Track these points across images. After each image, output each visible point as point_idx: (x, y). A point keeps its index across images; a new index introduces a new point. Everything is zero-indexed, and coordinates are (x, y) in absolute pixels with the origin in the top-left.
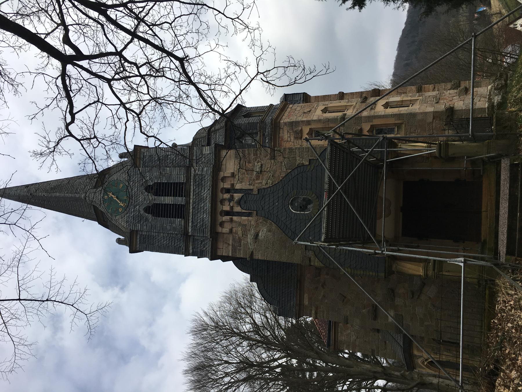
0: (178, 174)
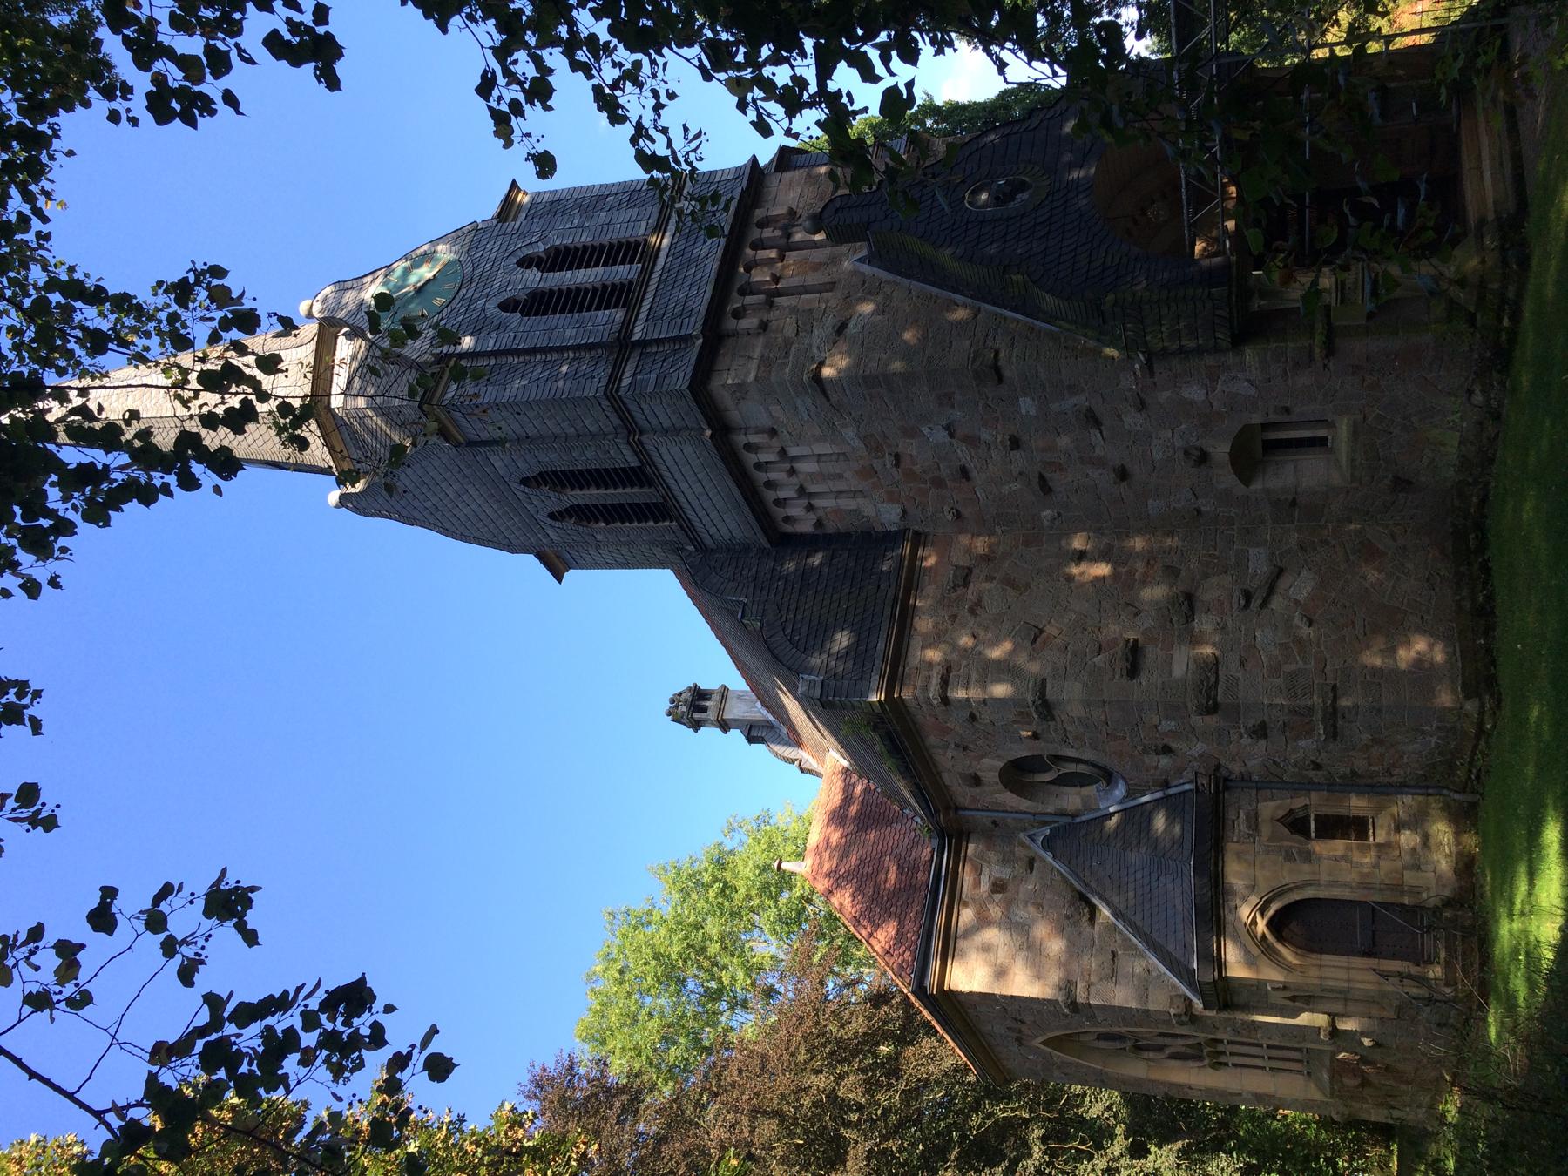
0: (632, 219)
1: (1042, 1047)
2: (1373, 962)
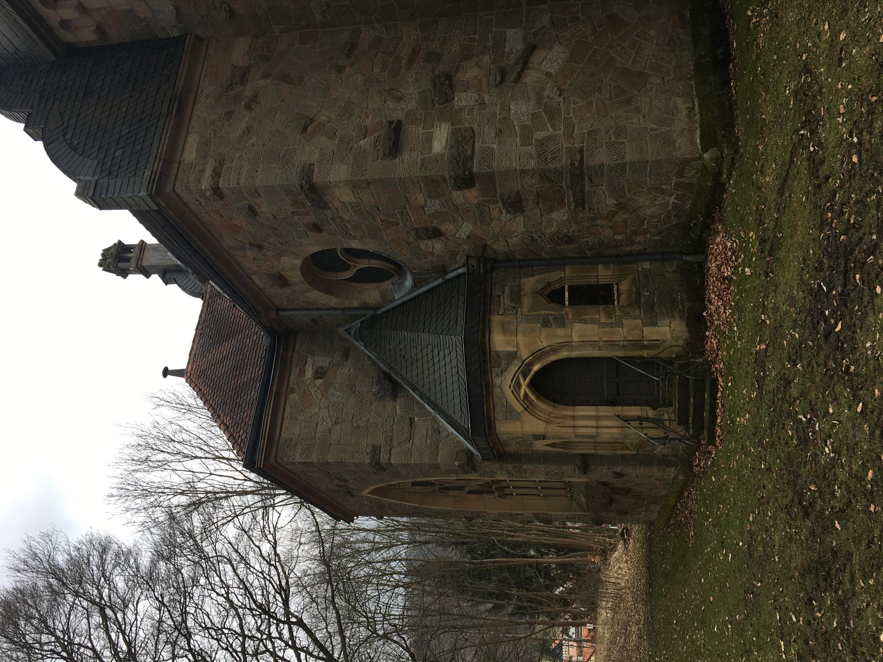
1: (368, 495)
2: (618, 410)
